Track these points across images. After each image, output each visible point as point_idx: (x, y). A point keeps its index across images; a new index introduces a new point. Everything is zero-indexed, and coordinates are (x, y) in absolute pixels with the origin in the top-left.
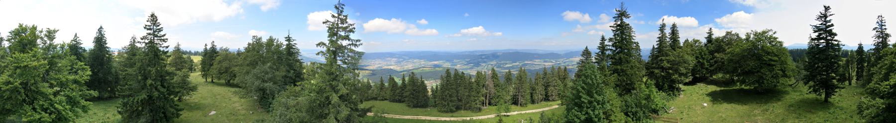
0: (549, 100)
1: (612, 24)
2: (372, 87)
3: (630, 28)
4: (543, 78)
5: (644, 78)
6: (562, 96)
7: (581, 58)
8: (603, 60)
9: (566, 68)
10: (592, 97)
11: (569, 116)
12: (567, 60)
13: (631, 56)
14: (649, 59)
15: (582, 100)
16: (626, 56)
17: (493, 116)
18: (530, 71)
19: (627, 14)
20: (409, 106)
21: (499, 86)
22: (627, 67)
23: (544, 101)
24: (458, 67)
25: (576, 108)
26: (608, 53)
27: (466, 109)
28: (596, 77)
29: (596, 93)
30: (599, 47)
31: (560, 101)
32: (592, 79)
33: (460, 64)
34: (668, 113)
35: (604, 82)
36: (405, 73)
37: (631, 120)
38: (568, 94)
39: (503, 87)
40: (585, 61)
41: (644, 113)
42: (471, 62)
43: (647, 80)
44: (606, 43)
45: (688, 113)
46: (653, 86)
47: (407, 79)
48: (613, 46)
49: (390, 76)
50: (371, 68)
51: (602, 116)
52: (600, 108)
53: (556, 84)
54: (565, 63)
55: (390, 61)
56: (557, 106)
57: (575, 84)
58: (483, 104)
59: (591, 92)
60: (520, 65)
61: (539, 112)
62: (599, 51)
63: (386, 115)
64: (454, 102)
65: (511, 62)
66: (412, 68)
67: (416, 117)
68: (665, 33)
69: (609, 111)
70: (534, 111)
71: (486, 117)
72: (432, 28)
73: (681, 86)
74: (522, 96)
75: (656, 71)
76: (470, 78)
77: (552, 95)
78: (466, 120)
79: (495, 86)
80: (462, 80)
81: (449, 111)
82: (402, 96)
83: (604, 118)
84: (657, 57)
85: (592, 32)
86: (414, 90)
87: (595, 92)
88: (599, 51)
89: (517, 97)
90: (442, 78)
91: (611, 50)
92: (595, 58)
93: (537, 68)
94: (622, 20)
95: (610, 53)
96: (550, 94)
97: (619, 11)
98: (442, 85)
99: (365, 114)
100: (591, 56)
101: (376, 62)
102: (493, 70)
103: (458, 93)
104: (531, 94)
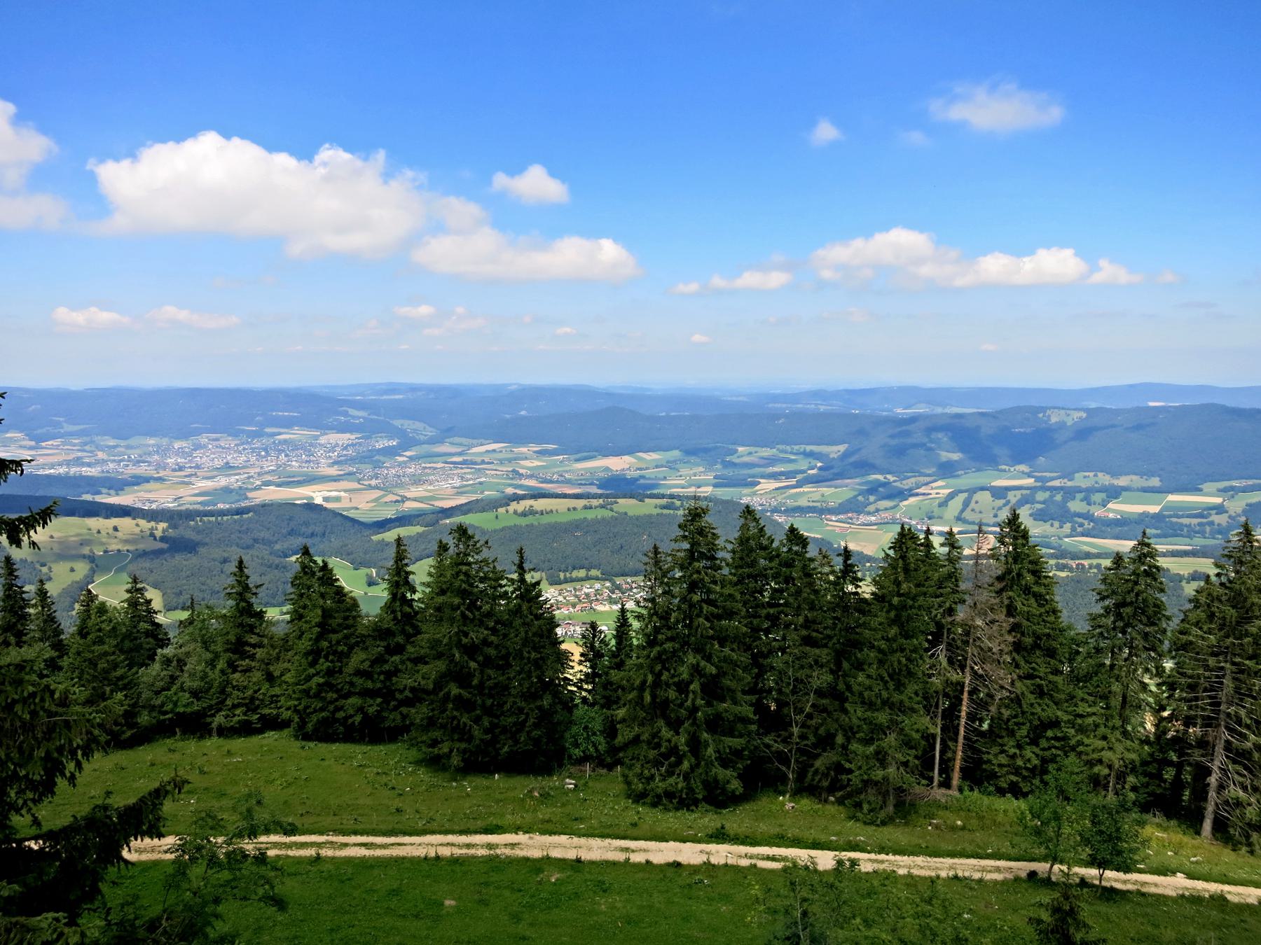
2: (164, 643)
20: (435, 763)
21: (1051, 653)
33: (774, 476)
36: (404, 531)
47: (421, 572)
49: (306, 552)
50: (163, 498)
55: (307, 448)
58: (927, 763)
63: (272, 844)
64: (731, 733)
65: (1155, 482)
66: (462, 500)
67: (479, 844)
71: (943, 867)
72: (593, 233)
76: (848, 571)
78: (811, 870)
79: (1018, 647)
80: (789, 579)
82: (387, 694)
86: (471, 651)
89: (1197, 756)
90: (656, 566)
98: (657, 614)
99: (111, 853)
101: (199, 457)
103: (762, 670)
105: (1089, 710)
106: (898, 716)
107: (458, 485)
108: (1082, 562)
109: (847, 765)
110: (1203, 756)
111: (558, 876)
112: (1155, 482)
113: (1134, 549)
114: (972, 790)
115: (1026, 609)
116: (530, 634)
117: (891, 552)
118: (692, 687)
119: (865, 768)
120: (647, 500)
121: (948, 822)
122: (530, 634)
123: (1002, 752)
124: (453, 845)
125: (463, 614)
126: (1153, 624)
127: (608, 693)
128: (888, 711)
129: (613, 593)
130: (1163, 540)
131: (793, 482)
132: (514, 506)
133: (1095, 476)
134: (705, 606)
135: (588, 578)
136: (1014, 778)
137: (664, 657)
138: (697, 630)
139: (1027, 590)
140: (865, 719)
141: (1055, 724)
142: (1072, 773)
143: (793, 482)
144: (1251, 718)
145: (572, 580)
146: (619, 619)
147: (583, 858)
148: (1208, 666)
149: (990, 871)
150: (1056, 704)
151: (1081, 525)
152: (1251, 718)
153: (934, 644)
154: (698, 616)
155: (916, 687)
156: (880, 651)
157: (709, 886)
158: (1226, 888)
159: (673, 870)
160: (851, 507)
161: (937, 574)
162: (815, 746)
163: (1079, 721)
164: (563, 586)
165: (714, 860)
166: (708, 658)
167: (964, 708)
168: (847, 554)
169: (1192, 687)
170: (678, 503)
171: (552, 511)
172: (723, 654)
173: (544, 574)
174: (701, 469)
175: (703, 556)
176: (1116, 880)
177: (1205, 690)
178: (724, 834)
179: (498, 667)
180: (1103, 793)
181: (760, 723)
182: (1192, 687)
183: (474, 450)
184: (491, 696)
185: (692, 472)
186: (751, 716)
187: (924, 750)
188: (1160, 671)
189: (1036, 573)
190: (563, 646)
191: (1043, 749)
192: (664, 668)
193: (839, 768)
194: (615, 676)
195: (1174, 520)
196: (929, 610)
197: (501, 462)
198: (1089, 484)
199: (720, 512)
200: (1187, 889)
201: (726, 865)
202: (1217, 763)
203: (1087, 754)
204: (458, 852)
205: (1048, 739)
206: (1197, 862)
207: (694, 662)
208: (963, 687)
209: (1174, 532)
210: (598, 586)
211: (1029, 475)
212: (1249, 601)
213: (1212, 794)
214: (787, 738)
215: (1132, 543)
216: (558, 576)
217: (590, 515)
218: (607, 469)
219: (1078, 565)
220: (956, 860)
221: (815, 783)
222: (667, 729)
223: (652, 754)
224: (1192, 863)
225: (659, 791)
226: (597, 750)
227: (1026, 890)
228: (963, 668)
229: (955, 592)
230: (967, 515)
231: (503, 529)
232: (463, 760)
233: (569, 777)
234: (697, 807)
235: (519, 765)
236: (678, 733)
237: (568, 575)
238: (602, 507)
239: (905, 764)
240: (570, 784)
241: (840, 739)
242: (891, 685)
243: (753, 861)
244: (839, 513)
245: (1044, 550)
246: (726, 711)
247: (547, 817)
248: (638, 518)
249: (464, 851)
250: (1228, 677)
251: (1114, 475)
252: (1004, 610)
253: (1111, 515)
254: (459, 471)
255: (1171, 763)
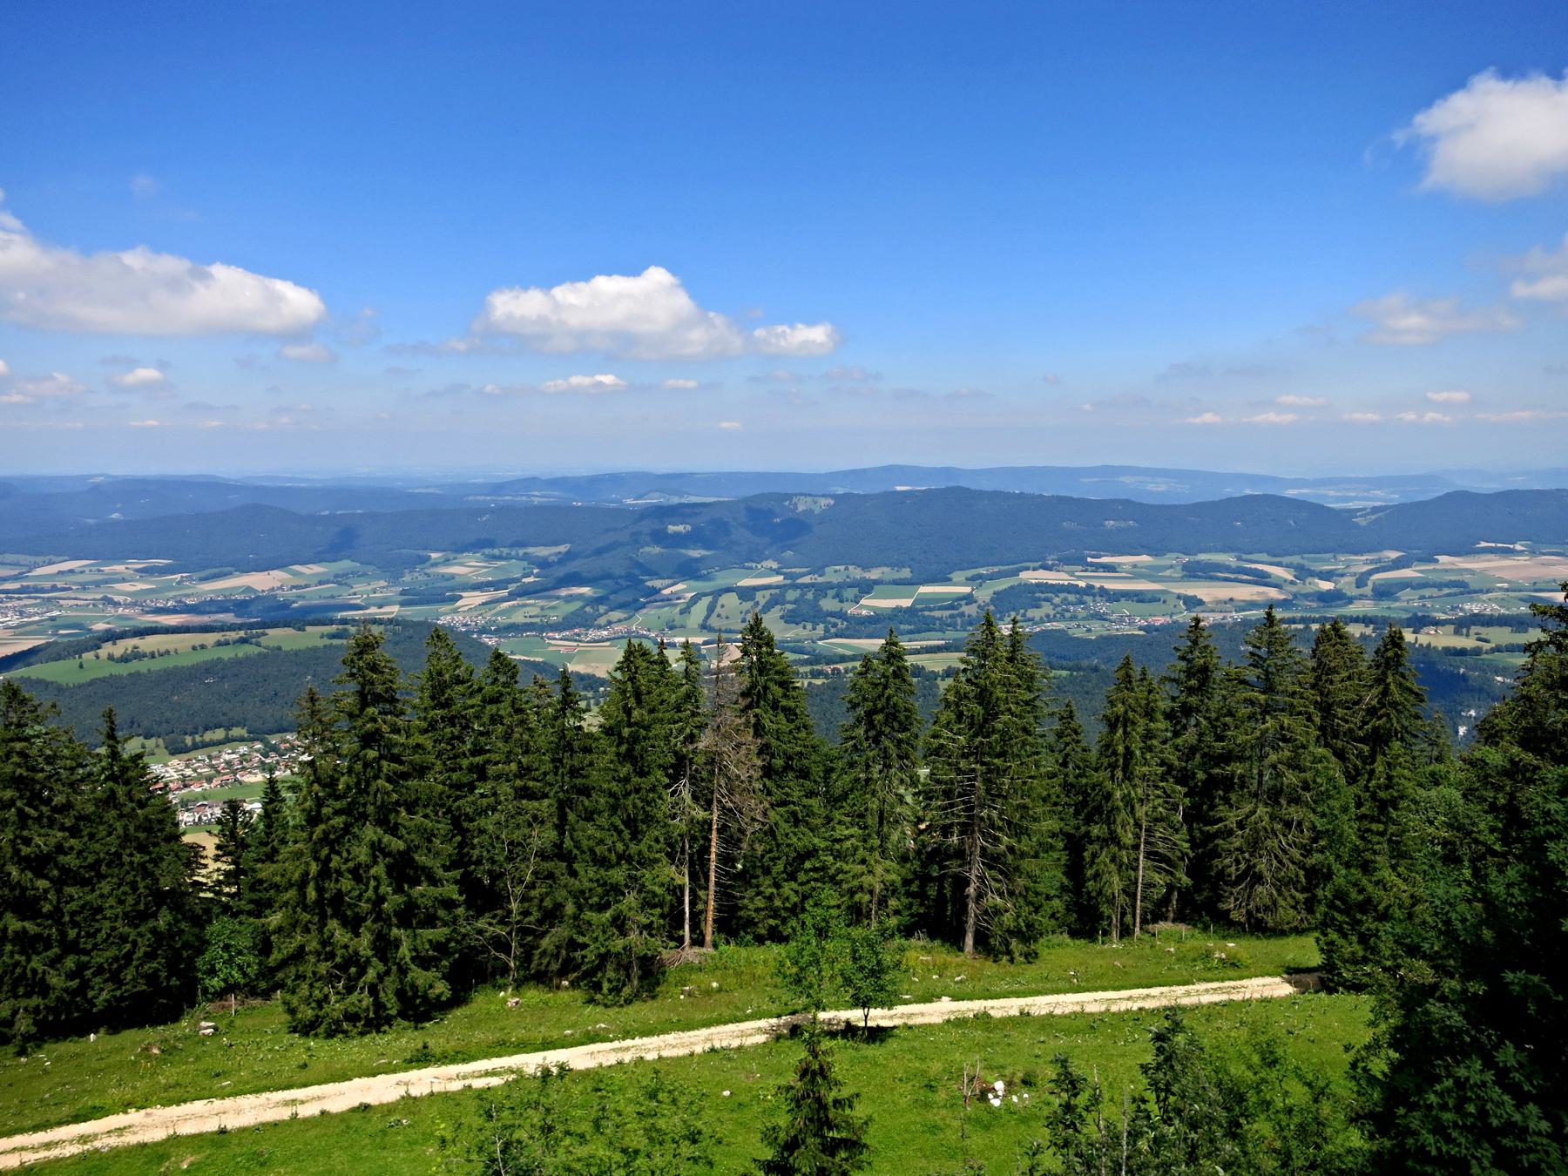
0: (1223, 923)
4: (1179, 716)
6: (1340, 895)
9: (1396, 641)
17: (750, 1033)
18: (1063, 648)
21: (804, 774)
23: (1180, 918)
24: (463, 615)
25: (1508, 1055)
27: (542, 978)
31: (1309, 941)
39: (841, 783)
42: (572, 567)
53: (1291, 778)
54: (1384, 593)
60: (984, 594)
61: (1138, 1017)
65: (906, 573)
70: (1093, 1002)
71: (697, 1041)
74: (992, 861)
76: (568, 702)
79: (768, 771)
81: (392, 1005)
89: (954, 867)
93: (1117, 630)
96: (1228, 864)
98: (321, 779)
102: (756, 635)
104: (1075, 845)
105: (846, 832)
106: (637, 870)
107: (15, 623)
108: (838, 666)
109: (581, 940)
110: (960, 866)
111: (193, 1159)
112: (906, 573)
113: (883, 648)
114: (728, 943)
115: (774, 726)
116: (132, 828)
117: (619, 675)
118: (373, 871)
119: (601, 938)
120: (308, 628)
121: (703, 986)
122: (132, 828)
123: (758, 894)
124: (23, 1149)
125: (20, 812)
126: (905, 729)
127: (255, 896)
128: (625, 866)
129: (266, 756)
130: (917, 636)
131: (504, 593)
132: (107, 649)
133: (847, 569)
134: (384, 763)
135: (228, 740)
136: (772, 922)
137: (332, 837)
138: (375, 796)
139: (775, 706)
140: (598, 881)
141: (812, 853)
142: (829, 907)
143: (504, 593)
144: (1003, 820)
145: (205, 745)
146: (266, 794)
147: (229, 1127)
148: (960, 769)
149: (750, 1035)
150: (812, 830)
151: (835, 625)
152: (1003, 820)
153: (675, 779)
154: (376, 777)
155: (657, 833)
156: (611, 794)
157: (409, 1126)
158: (990, 1003)
159: (358, 1116)
160: (578, 622)
161: (673, 696)
162: (540, 922)
163: (837, 846)
164: (191, 755)
165: (414, 1092)
166: (393, 830)
167: (713, 850)
168: (565, 679)
169: (947, 794)
170: (353, 630)
171: (168, 652)
172: (413, 823)
173: (161, 741)
174: (383, 583)
175: (378, 699)
176: (883, 1018)
177: (960, 795)
178: (426, 1055)
179: (84, 882)
180: (866, 922)
181: (469, 904)
182: (947, 794)
183: (39, 571)
184: (75, 924)
185: (369, 588)
186: (455, 897)
187: (672, 906)
188: (914, 781)
189: (784, 685)
190: (186, 839)
191: (802, 884)
192: (333, 851)
193: (573, 945)
194: (266, 871)
195: (927, 613)
196: (667, 738)
197: (84, 587)
198: (840, 580)
199: (411, 637)
200: (953, 1012)
201: (432, 1094)
202: (974, 872)
203: (848, 882)
204: (30, 1158)
205: (807, 871)
206: (961, 982)
207: (375, 838)
208: (710, 825)
209: (926, 626)
210: (243, 749)
211: (778, 572)
212: (994, 696)
213: (971, 905)
214: (504, 917)
215: (883, 641)
216: (183, 741)
217: (227, 654)
218: (249, 589)
219: (833, 670)
220: (713, 1030)
221: (543, 968)
222: (343, 931)
223: (323, 968)
224: (957, 983)
225: (335, 1015)
226: (245, 975)
227: (790, 1048)
228: (709, 803)
229: (694, 714)
230: (714, 622)
231: (92, 683)
232: (36, 1023)
233: (205, 1019)
234: (390, 1026)
235: (120, 1018)
236: (358, 935)
237: (198, 738)
238: (243, 641)
239: (649, 927)
240: (207, 1028)
241: (570, 908)
242: (627, 835)
243: (467, 1082)
244: (565, 630)
245: (791, 656)
246: (423, 896)
247: (172, 1081)
248: (297, 653)
249: (42, 1154)
250: (979, 779)
251: (865, 568)
252: (751, 731)
253: (864, 612)
254: (16, 603)
255: (933, 879)
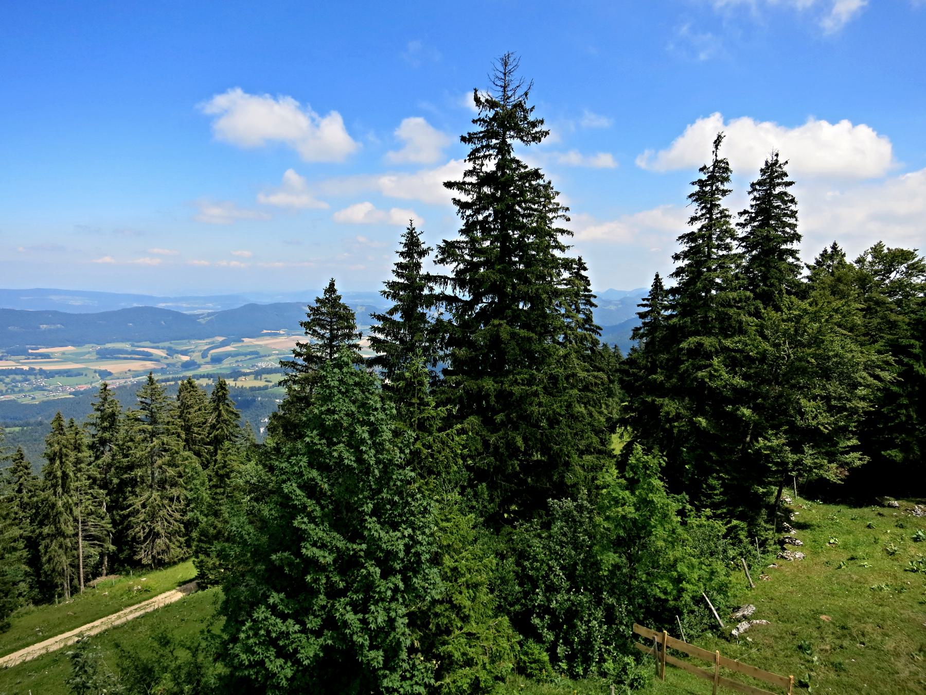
0: (138, 566)
1: (458, 170)
3: (545, 194)
4: (97, 447)
5: (615, 438)
6: (203, 533)
7: (305, 340)
8: (410, 348)
9: (222, 386)
10: (355, 535)
11: (237, 649)
12: (228, 349)
13: (546, 331)
14: (636, 344)
15: (309, 551)
16: (523, 333)
19: (531, 118)
22: (531, 381)
23: (111, 571)
25: (275, 598)
26: (433, 314)
28: (374, 431)
29: (373, 513)
30: (392, 285)
32: (355, 445)
34: (730, 638)
35: (414, 459)
37: (545, 657)
38: (238, 523)
40: (324, 354)
41: (610, 618)
43: (628, 449)
44: (428, 266)
45: (838, 659)
46: (657, 482)
48: (459, 280)
51: (406, 636)
52: (396, 590)
53: (171, 472)
54: (217, 360)
56: (176, 596)
57: (271, 469)
59: (351, 508)
62: (392, 303)
68: (724, 215)
69: (438, 609)
73: (789, 497)
75: (670, 406)
77: (153, 535)
83: (412, 650)
84: (676, 333)
85: (360, 212)
87: (369, 507)
88: (392, 303)
91: (451, 300)
92: (374, 340)
94: (503, 149)
95: (447, 317)
97: (492, 104)
100: (352, 328)
104: (32, 543)
